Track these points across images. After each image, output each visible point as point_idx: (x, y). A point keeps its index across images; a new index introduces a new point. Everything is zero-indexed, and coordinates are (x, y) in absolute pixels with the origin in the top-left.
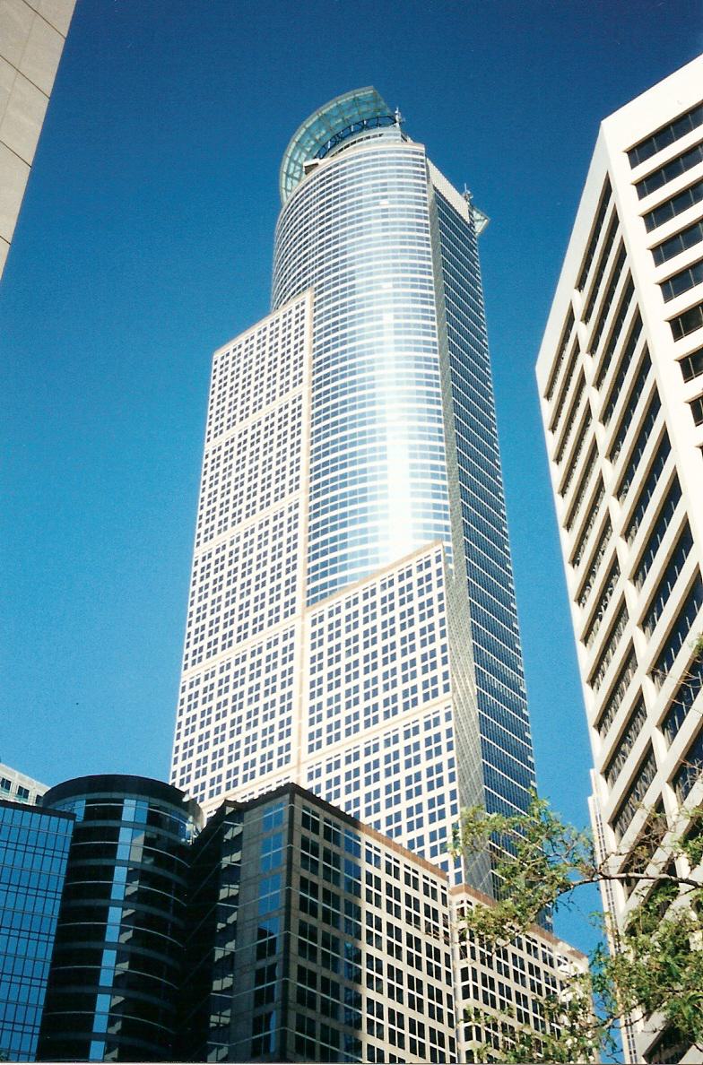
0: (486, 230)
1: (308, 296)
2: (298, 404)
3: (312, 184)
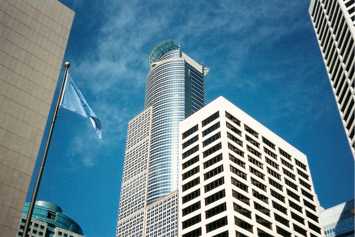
1: (151, 108)
2: (150, 111)
3: (154, 71)
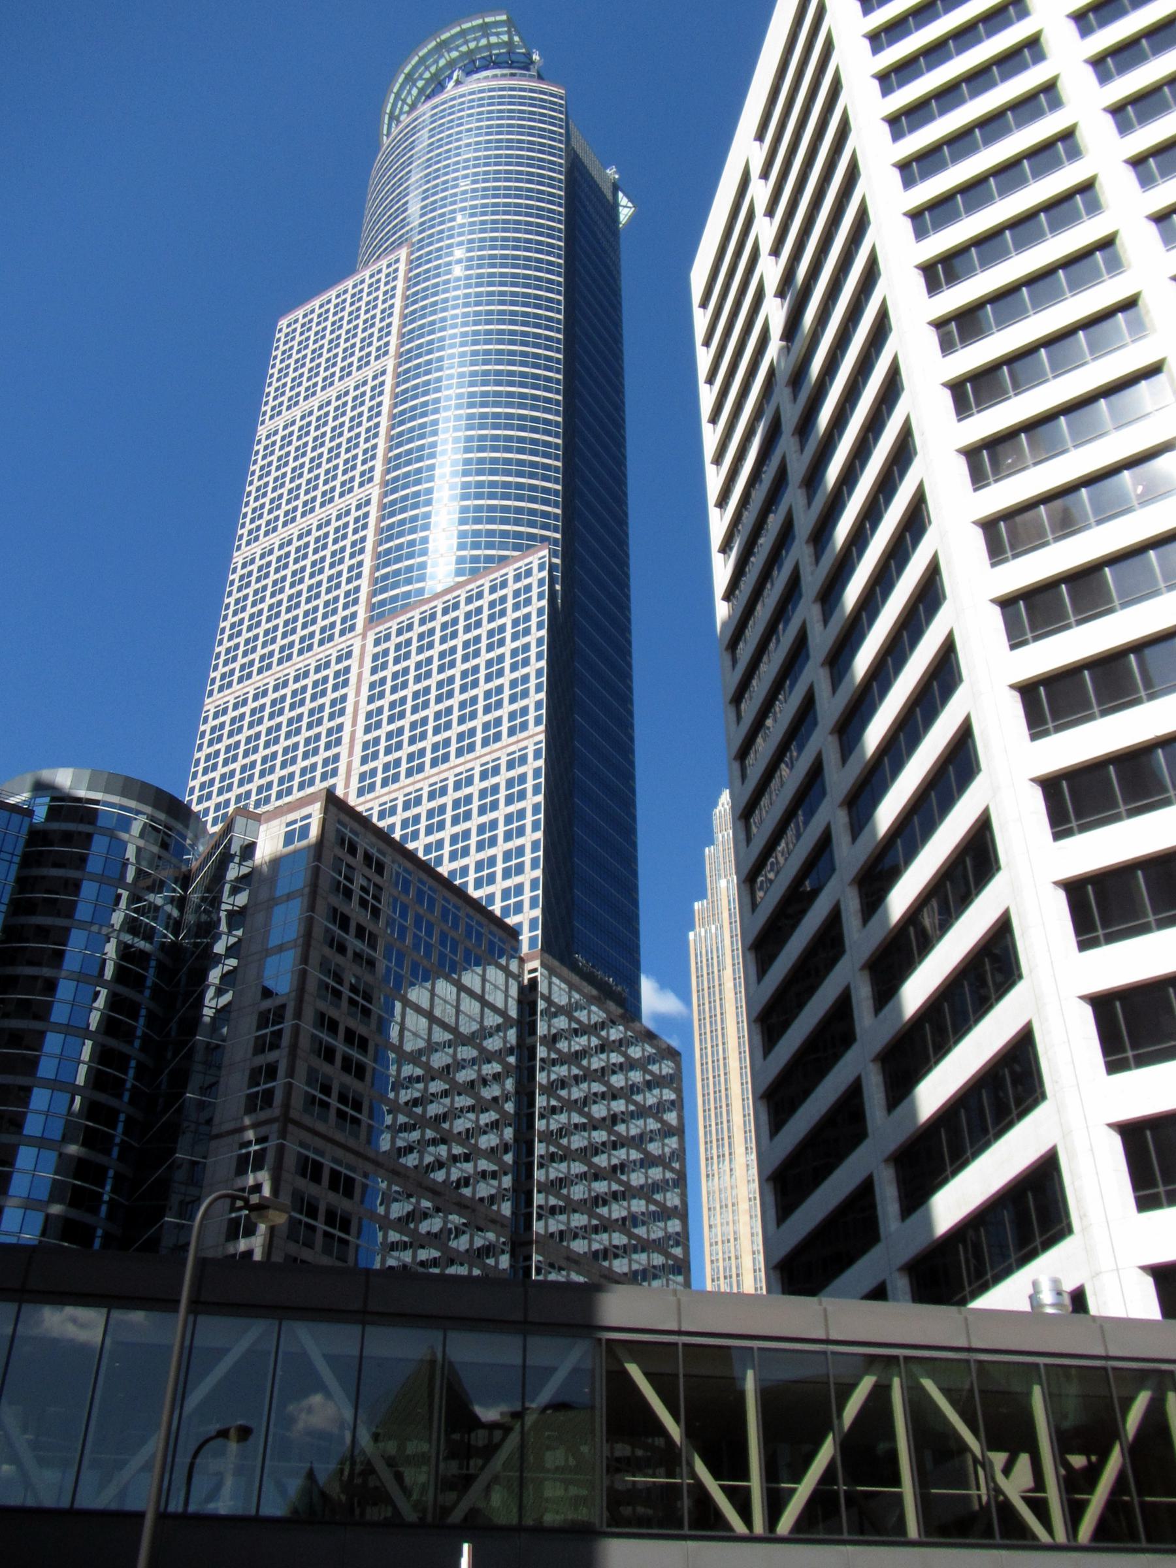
0: (633, 218)
1: (403, 253)
